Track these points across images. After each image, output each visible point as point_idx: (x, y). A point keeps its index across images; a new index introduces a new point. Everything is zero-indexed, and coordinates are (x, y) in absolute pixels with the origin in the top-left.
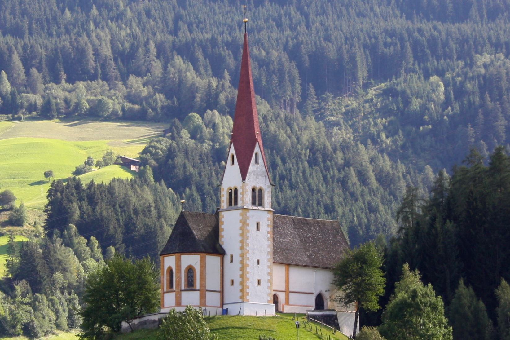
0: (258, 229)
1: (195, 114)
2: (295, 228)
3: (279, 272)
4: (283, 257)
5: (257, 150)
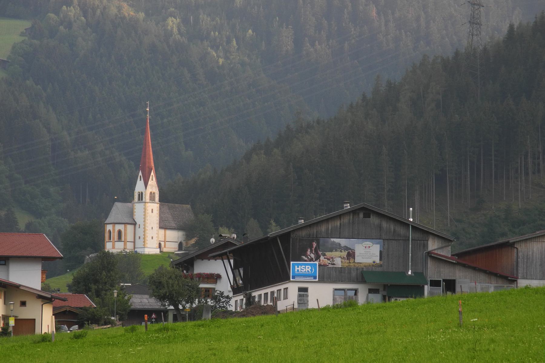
0: (152, 212)
1: (49, 14)
2: (169, 209)
3: (162, 231)
4: (163, 225)
5: (152, 174)
